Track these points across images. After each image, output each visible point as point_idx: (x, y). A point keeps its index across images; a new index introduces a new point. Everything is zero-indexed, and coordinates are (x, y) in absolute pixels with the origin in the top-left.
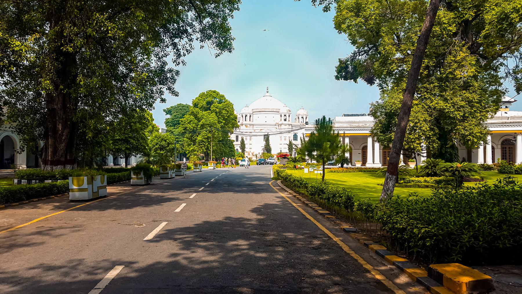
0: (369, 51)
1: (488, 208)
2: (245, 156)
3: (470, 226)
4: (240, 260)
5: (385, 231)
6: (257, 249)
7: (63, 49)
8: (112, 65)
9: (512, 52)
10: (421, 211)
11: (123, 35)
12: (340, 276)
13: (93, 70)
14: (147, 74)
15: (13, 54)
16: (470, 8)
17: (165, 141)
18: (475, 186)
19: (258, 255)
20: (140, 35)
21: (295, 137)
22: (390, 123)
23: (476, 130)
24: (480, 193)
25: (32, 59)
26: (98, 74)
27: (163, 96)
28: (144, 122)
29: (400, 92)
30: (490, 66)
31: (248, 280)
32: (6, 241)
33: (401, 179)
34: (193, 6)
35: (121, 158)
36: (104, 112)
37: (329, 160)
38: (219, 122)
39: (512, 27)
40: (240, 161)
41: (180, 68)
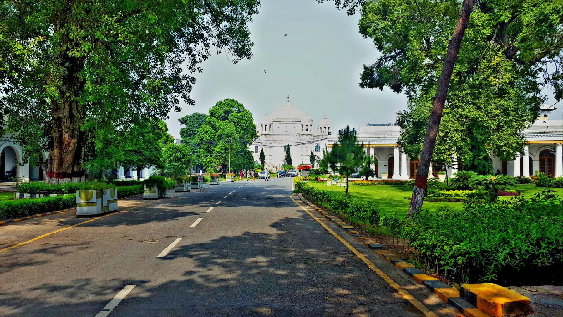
0: (396, 57)
1: (525, 224)
2: (265, 168)
3: (505, 243)
4: (259, 278)
5: (413, 248)
6: (277, 266)
7: (69, 54)
8: (123, 71)
9: (552, 56)
10: (453, 225)
11: (134, 39)
12: (366, 295)
13: (102, 76)
14: (160, 81)
15: (14, 59)
16: (506, 9)
17: (181, 152)
18: (510, 201)
19: (279, 272)
20: (152, 39)
21: (317, 148)
22: (418, 132)
23: (512, 140)
24: (517, 208)
25: (35, 64)
26: (107, 80)
27: (177, 105)
28: (160, 132)
29: (429, 101)
30: (528, 71)
31: (267, 299)
32: (7, 260)
33: (430, 192)
34: (209, 8)
35: (133, 170)
36: (114, 122)
37: (354, 172)
38: (237, 132)
39: (552, 29)
40: (259, 174)
41: (196, 75)
